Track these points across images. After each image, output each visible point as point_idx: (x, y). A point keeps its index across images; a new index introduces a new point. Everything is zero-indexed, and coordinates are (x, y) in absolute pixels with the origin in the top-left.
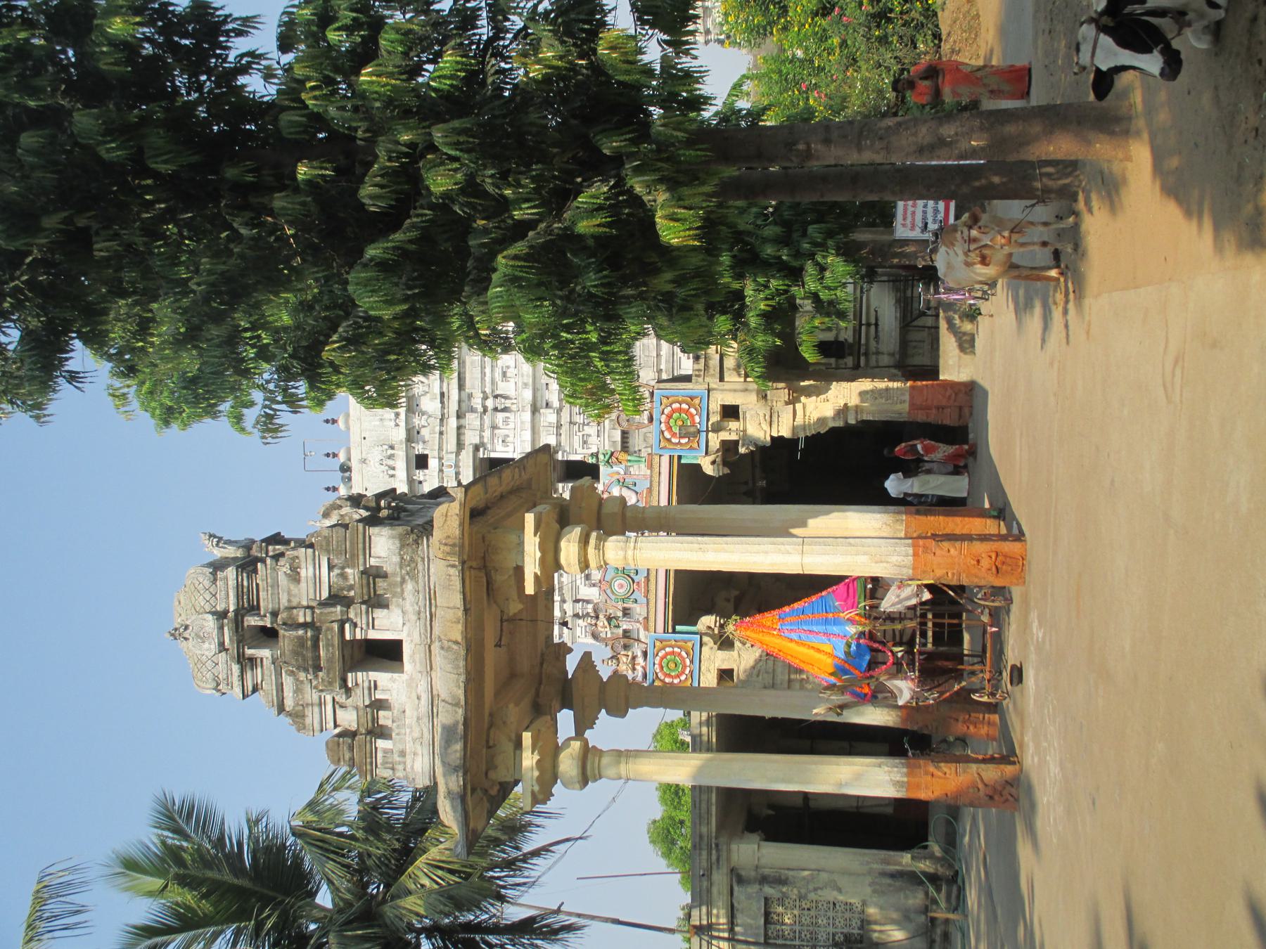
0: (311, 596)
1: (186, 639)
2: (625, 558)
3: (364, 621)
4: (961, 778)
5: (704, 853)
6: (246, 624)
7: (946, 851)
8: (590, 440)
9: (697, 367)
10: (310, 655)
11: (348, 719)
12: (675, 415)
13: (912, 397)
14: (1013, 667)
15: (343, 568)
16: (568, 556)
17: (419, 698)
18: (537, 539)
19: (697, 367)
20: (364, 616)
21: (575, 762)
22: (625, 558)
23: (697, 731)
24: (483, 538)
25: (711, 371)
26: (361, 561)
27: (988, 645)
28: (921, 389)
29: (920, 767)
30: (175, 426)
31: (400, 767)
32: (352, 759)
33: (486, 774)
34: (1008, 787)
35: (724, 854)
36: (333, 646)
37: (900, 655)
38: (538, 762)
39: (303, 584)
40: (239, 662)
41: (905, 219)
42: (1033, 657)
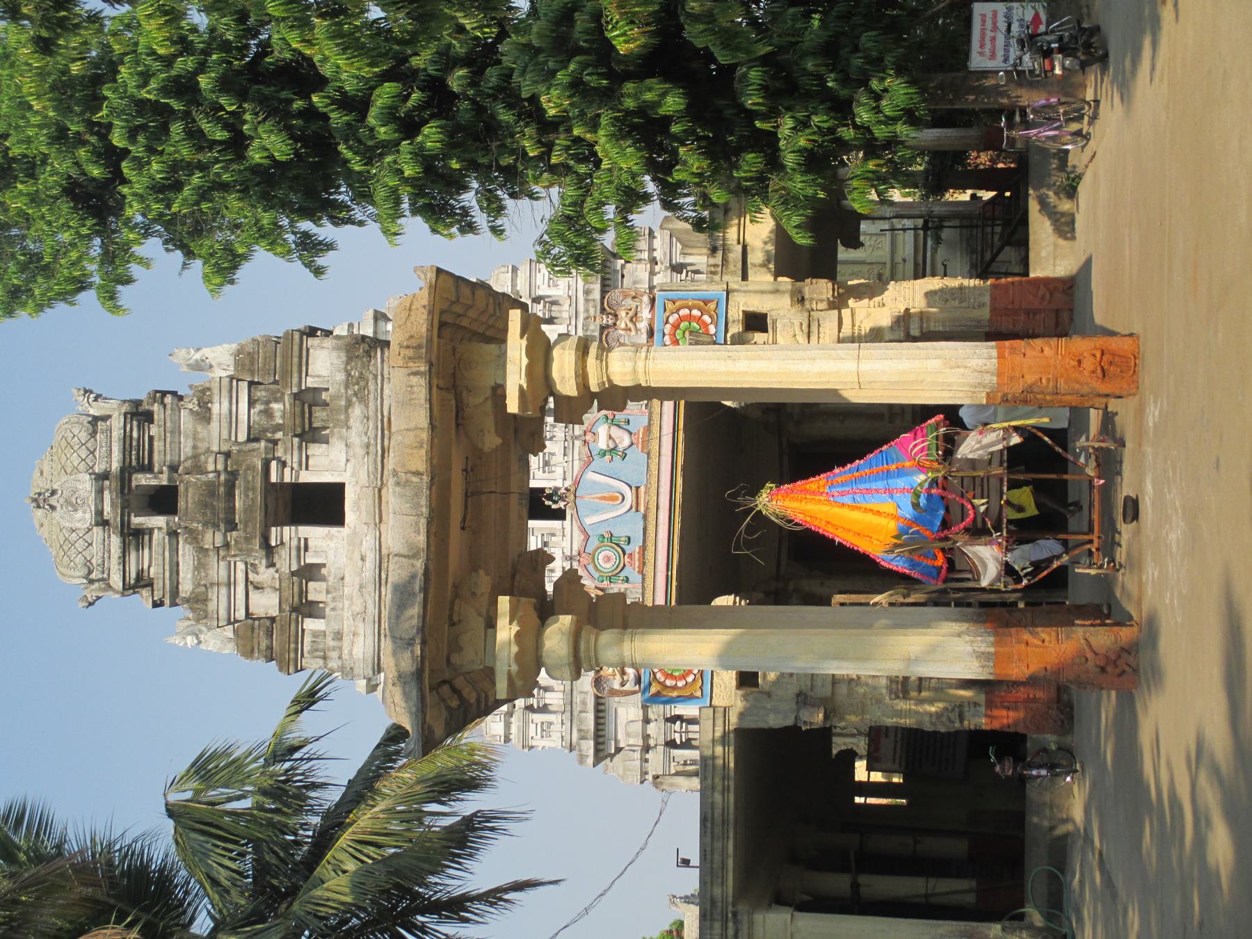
0: (225, 435)
1: (53, 508)
2: (635, 371)
3: (296, 459)
4: (1064, 646)
5: (717, 925)
6: (134, 484)
7: (1049, 917)
8: (553, 460)
9: (712, 261)
10: (222, 505)
11: (266, 604)
12: (683, 325)
13: (993, 299)
14: (1127, 498)
15: (267, 403)
16: (562, 367)
17: (363, 559)
18: (524, 342)
19: (712, 261)
20: (296, 453)
21: (565, 638)
22: (635, 371)
23: (708, 753)
24: (454, 350)
25: (731, 267)
26: (295, 380)
27: (1096, 503)
28: (1006, 286)
29: (1011, 636)
30: (23, 315)
31: (334, 654)
32: (270, 648)
33: (448, 660)
34: (1124, 655)
35: (744, 928)
36: (254, 489)
37: (982, 509)
38: (518, 635)
39: (214, 424)
40: (122, 534)
41: (982, 46)
42: (1149, 488)
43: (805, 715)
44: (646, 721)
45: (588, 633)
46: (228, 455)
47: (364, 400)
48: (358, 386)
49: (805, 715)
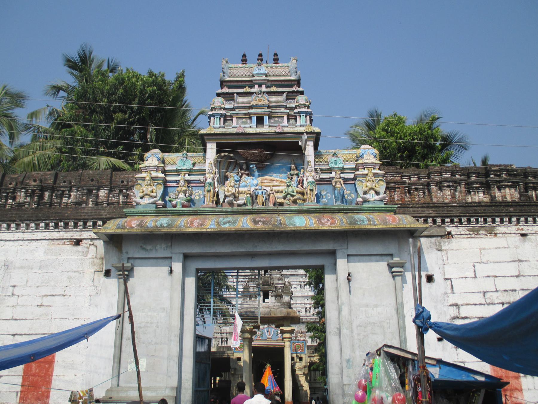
43: (233, 370)
44: (226, 333)
45: (248, 340)
46: (273, 284)
47: (282, 305)
48: (283, 304)
49: (233, 370)
